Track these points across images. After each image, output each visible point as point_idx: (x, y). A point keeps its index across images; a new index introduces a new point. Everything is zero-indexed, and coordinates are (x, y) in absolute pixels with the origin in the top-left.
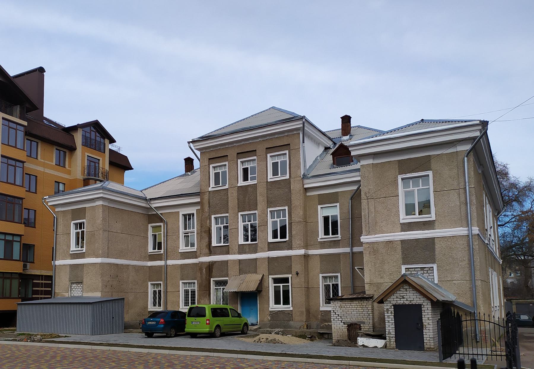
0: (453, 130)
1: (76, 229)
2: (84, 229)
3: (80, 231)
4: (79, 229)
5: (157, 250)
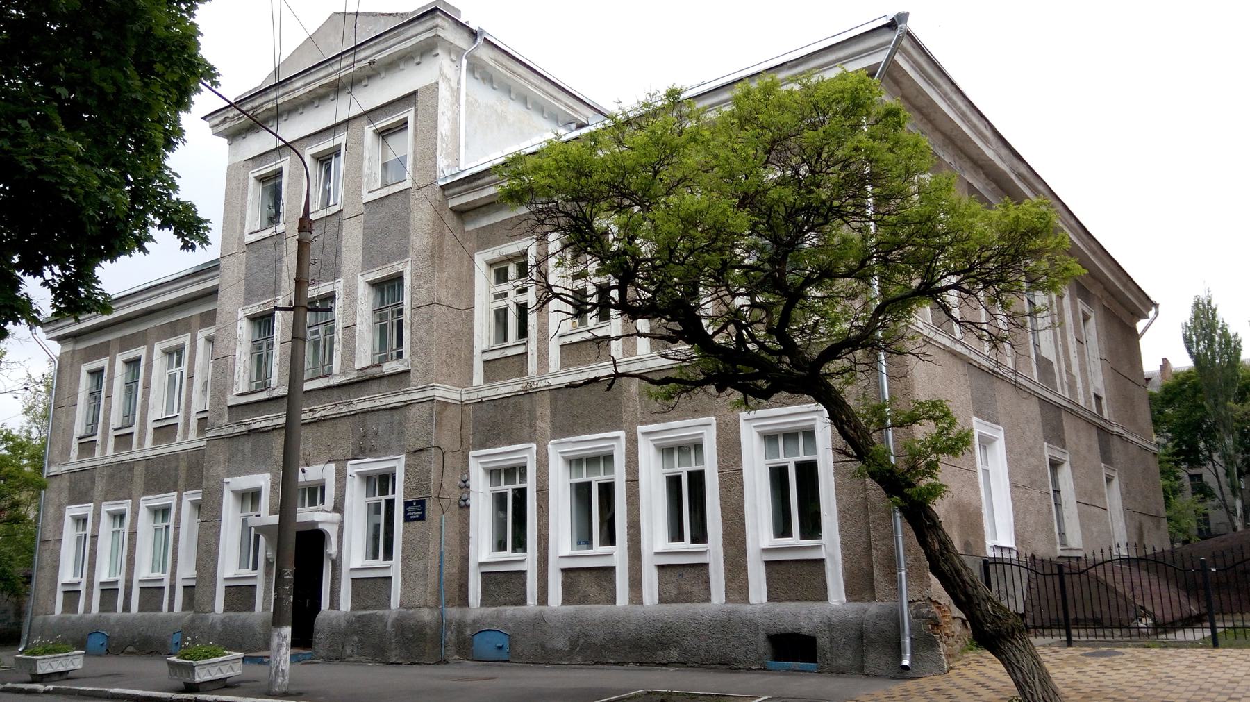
0: (841, 49)
1: (370, 492)
2: (393, 493)
3: (382, 499)
4: (380, 495)
5: (795, 540)
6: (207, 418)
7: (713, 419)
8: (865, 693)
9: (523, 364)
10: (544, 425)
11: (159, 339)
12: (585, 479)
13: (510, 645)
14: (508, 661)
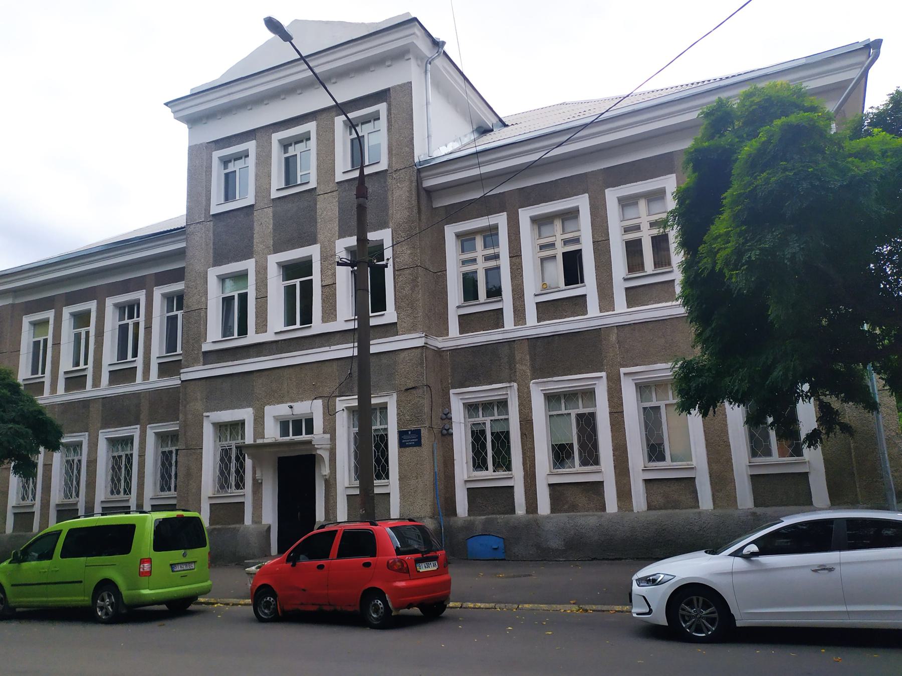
6: (181, 360)
9: (498, 318)
10: (524, 368)
11: (111, 294)
12: (654, 403)
13: (505, 546)
14: (504, 560)
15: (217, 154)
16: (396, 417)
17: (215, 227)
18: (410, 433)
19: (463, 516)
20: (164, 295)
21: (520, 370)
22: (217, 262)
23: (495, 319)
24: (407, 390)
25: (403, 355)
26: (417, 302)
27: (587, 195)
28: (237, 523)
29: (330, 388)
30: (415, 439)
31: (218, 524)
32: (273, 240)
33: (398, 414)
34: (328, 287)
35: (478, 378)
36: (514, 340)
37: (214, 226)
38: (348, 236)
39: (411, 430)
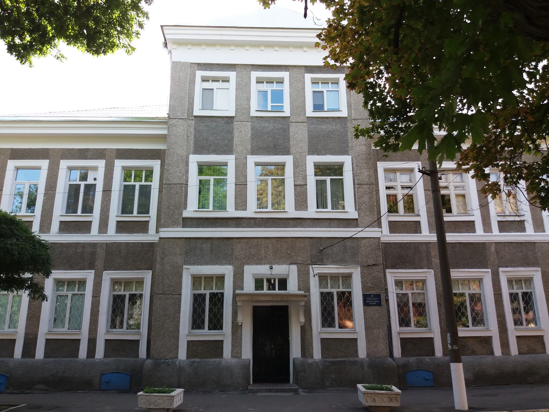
5: (413, 328)
7: (489, 270)
8: (142, 409)
15: (199, 74)
16: (361, 284)
17: (196, 125)
18: (372, 296)
19: (398, 357)
20: (124, 168)
21: (435, 262)
22: (199, 150)
23: (143, 227)
24: (368, 266)
25: (364, 242)
26: (373, 208)
27: (48, 160)
28: (215, 357)
29: (303, 257)
30: (377, 301)
31: (195, 357)
32: (251, 145)
33: (362, 282)
34: (299, 186)
35: (405, 264)
36: (430, 243)
37: (195, 124)
38: (316, 155)
39: (373, 294)
